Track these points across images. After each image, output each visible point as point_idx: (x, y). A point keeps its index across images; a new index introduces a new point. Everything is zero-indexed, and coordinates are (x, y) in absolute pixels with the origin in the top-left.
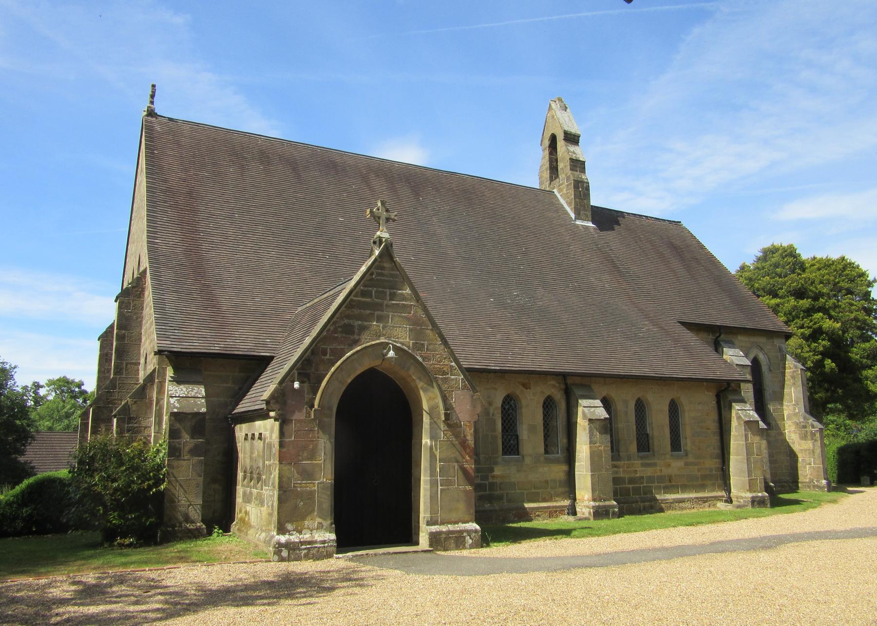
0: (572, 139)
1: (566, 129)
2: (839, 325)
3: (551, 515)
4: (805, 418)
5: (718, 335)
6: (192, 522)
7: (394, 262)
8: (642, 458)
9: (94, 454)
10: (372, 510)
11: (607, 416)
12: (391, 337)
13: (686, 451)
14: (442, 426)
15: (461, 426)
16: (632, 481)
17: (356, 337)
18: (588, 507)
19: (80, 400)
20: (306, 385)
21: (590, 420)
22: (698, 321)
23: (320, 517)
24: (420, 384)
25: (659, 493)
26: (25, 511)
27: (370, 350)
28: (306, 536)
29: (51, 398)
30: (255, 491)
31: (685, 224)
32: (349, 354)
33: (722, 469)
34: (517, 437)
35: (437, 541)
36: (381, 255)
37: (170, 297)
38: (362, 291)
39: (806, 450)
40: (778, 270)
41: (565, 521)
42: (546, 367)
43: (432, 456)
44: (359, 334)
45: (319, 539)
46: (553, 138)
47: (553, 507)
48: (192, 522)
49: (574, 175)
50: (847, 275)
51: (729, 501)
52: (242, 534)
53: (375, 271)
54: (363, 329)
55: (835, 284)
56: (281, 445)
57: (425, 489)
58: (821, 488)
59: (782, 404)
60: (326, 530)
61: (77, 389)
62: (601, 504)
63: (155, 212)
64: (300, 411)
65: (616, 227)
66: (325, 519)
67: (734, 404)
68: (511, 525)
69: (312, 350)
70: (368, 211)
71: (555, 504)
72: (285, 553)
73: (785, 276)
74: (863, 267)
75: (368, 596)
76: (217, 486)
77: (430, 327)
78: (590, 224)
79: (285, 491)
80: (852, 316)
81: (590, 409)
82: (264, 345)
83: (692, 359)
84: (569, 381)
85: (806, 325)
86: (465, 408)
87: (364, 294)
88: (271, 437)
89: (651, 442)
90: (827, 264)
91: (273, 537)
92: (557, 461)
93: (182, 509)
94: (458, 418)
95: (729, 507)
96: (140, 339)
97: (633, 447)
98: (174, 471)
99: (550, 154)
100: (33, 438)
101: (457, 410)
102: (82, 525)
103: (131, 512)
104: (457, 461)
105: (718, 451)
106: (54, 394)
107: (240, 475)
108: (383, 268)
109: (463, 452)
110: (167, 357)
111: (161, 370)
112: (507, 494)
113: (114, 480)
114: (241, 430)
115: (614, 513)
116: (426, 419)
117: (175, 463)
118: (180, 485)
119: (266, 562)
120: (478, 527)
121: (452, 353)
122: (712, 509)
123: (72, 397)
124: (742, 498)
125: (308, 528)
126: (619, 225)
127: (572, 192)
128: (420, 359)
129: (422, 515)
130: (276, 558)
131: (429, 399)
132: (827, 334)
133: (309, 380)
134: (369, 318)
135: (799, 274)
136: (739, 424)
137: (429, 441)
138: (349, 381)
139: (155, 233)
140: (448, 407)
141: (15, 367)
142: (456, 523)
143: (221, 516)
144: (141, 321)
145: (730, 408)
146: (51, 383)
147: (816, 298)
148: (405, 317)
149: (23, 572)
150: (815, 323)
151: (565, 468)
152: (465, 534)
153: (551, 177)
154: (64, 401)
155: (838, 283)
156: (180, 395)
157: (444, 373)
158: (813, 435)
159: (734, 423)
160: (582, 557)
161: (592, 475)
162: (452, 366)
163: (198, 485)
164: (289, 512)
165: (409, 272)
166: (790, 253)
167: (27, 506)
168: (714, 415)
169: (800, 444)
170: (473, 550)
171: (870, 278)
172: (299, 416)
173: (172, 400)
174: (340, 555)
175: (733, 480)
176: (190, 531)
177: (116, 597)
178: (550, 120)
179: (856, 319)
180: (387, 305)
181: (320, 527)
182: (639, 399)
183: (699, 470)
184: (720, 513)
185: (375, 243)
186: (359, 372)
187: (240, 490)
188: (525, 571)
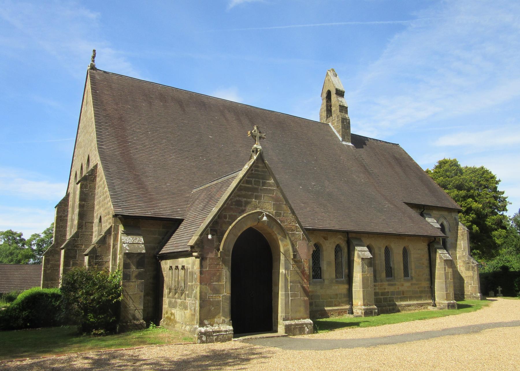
0: (340, 93)
2: (481, 206)
3: (339, 314)
4: (469, 258)
5: (423, 210)
6: (138, 320)
7: (265, 163)
8: (388, 281)
9: (77, 279)
10: (252, 313)
11: (372, 256)
12: (265, 208)
14: (291, 261)
15: (302, 262)
16: (383, 294)
17: (243, 208)
18: (361, 309)
19: (20, 245)
20: (215, 236)
21: (363, 259)
22: (412, 202)
24: (279, 237)
26: (25, 313)
28: (216, 328)
30: (179, 301)
31: (401, 145)
33: (431, 287)
34: (320, 268)
35: (289, 330)
36: (257, 159)
37: (117, 182)
38: (247, 180)
39: (469, 277)
40: (448, 174)
41: (347, 318)
42: (337, 227)
44: (245, 207)
45: (224, 329)
46: (329, 93)
47: (341, 309)
48: (138, 320)
49: (341, 115)
50: (485, 177)
51: (435, 305)
52: (170, 327)
54: (247, 203)
55: (478, 182)
56: (201, 273)
59: (456, 250)
60: (227, 324)
62: (368, 307)
63: (101, 129)
64: (212, 252)
65: (364, 146)
66: (226, 318)
68: (318, 320)
69: (219, 216)
70: (249, 132)
71: (341, 308)
72: (204, 338)
73: (452, 177)
74: (493, 173)
75: (272, 363)
76: (149, 298)
77: (285, 203)
78: (350, 144)
80: (487, 201)
81: (361, 253)
82: (177, 212)
83: (410, 224)
84: (350, 235)
85: (463, 205)
86: (305, 252)
87: (248, 182)
88: (193, 268)
89: (393, 271)
90: (474, 171)
91: (196, 328)
92: (342, 283)
93: (131, 312)
94: (300, 257)
95: (435, 309)
96: (94, 207)
97: (384, 275)
98: (127, 289)
99: (327, 102)
101: (300, 252)
102: (67, 321)
103: (100, 314)
104: (300, 283)
105: (429, 277)
107: (166, 291)
108: (258, 167)
109: (303, 278)
110: (119, 218)
111: (116, 227)
112: (315, 302)
113: (91, 294)
114: (166, 264)
115: (375, 313)
116: (282, 258)
117: (127, 284)
118: (130, 297)
119: (193, 343)
120: (311, 322)
121: (297, 219)
122: (426, 310)
124: (442, 304)
125: (217, 323)
126: (366, 145)
128: (279, 222)
130: (199, 341)
131: (285, 246)
132: (474, 210)
133: (217, 233)
134: (250, 197)
135: (459, 176)
136: (441, 261)
137: (284, 271)
138: (239, 234)
139: (102, 142)
140: (295, 251)
142: (299, 319)
143: (154, 315)
144: (94, 196)
145: (436, 252)
147: (468, 190)
148: (271, 197)
149: (48, 351)
150: (468, 204)
151: (347, 286)
152: (304, 326)
153: (327, 116)
154: (10, 245)
155: (480, 181)
156: (128, 242)
157: (292, 230)
158: (473, 268)
159: (438, 261)
160: (375, 338)
161: (363, 291)
162: (296, 226)
163: (140, 297)
164: (206, 313)
166: (454, 164)
167: (25, 311)
168: (426, 256)
169: (465, 273)
170: (309, 335)
171: (497, 179)
172: (211, 255)
173: (124, 245)
174: (236, 339)
175: (437, 294)
176: (136, 325)
177: (118, 366)
178: (327, 82)
179: (489, 202)
181: (224, 322)
183: (418, 288)
184: (432, 312)
185: (253, 151)
186: (245, 229)
187: (166, 301)
188: (352, 347)
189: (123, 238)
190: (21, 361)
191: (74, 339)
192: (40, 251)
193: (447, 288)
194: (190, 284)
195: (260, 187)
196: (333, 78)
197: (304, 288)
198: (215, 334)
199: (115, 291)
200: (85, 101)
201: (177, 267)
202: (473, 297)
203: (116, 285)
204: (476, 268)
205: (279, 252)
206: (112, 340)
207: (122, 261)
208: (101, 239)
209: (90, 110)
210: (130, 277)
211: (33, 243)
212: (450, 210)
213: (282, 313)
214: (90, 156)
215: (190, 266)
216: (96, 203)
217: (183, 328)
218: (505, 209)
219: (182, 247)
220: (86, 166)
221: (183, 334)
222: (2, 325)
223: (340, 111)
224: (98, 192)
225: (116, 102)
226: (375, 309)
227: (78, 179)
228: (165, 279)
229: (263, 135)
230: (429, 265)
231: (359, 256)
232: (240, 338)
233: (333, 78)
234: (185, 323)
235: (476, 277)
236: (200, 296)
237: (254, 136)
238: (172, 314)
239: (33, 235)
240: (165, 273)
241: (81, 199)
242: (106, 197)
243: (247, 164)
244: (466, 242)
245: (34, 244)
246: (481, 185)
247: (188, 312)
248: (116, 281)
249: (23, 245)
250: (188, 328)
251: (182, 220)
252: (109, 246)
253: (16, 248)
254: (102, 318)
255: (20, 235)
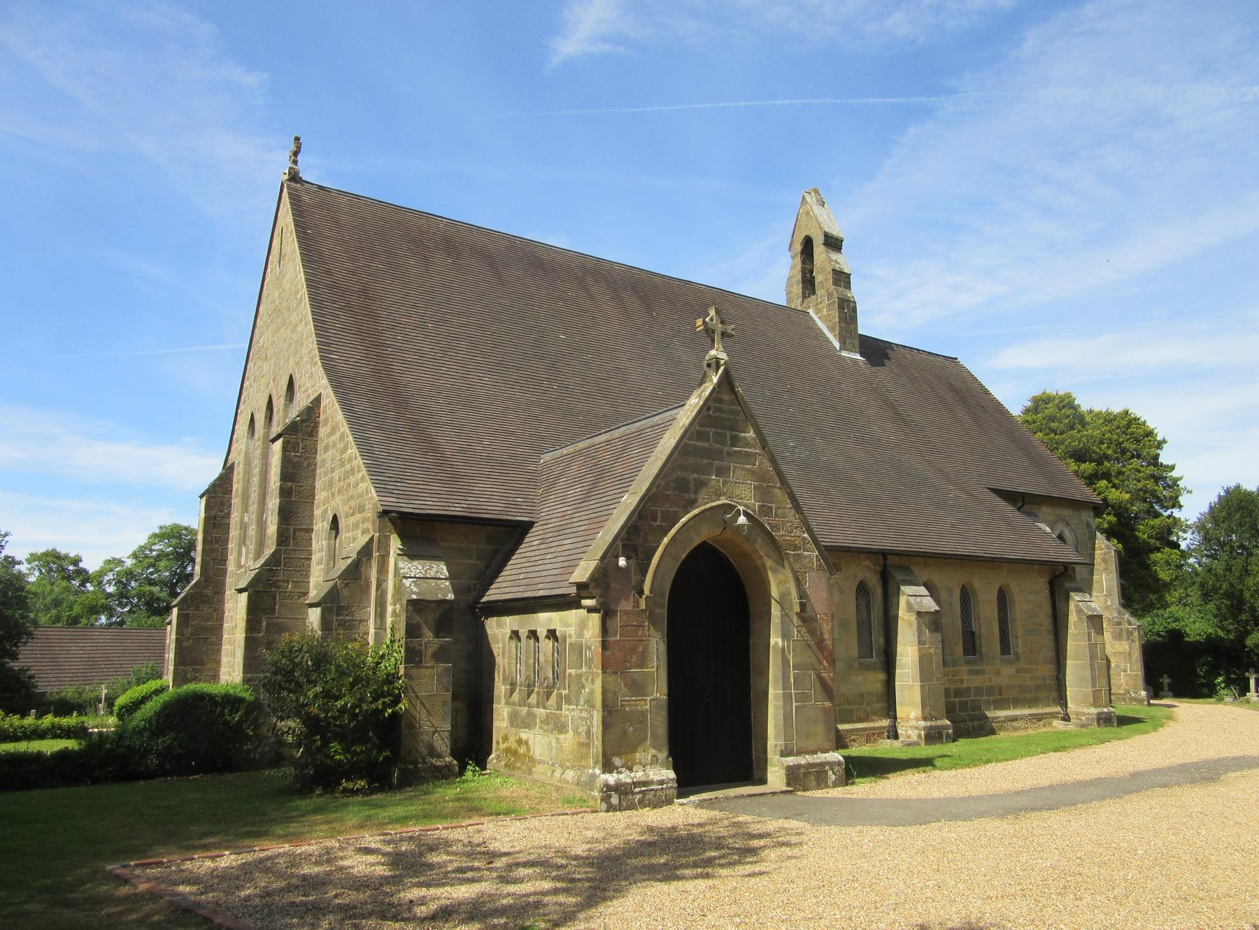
0: (833, 243)
1: (827, 230)
4: (1119, 613)
6: (439, 756)
7: (735, 394)
8: (969, 663)
12: (738, 495)
13: (1017, 654)
14: (795, 619)
16: (958, 693)
17: (692, 496)
18: (917, 728)
19: (76, 583)
20: (633, 561)
21: (919, 613)
23: (655, 748)
24: (769, 563)
25: (989, 709)
26: (163, 742)
27: (708, 514)
28: (639, 775)
29: (32, 579)
30: (540, 712)
31: (963, 361)
32: (684, 520)
35: (796, 778)
38: (698, 432)
39: (1120, 653)
41: (885, 748)
42: (861, 542)
43: (785, 661)
44: (696, 493)
45: (656, 778)
46: (808, 244)
48: (439, 756)
51: (1066, 718)
52: (517, 773)
53: (712, 404)
54: (701, 484)
56: (605, 645)
57: (776, 707)
58: (1139, 701)
60: (662, 765)
61: (71, 568)
62: (934, 723)
64: (627, 599)
65: (886, 361)
66: (660, 751)
67: (1072, 594)
70: (699, 322)
72: (615, 800)
73: (1062, 433)
74: (1151, 424)
79: (610, 712)
81: (913, 600)
87: (700, 436)
88: (581, 634)
89: (977, 642)
90: (1108, 419)
91: (594, 777)
92: (871, 668)
95: (1070, 727)
96: (313, 495)
97: (959, 650)
99: (803, 262)
100: (30, 634)
104: (814, 669)
106: (37, 573)
107: (500, 689)
108: (721, 401)
109: (820, 656)
113: (337, 698)
116: (775, 611)
117: (415, 672)
118: (422, 703)
119: (593, 812)
123: (64, 578)
124: (1084, 714)
125: (640, 763)
127: (835, 314)
129: (771, 742)
131: (780, 583)
132: (1113, 507)
134: (706, 470)
136: (1080, 619)
137: (780, 641)
138: (684, 556)
140: (802, 595)
141: (6, 535)
142: (815, 752)
143: (474, 744)
144: (314, 470)
145: (1067, 598)
146: (33, 558)
147: (1099, 463)
148: (748, 470)
151: (882, 676)
152: (827, 768)
153: (804, 293)
154: (52, 584)
157: (796, 548)
158: (1130, 633)
159: (1073, 618)
161: (922, 686)
164: (616, 744)
165: (756, 410)
166: (1067, 403)
167: (164, 735)
168: (1047, 608)
171: (1159, 438)
173: (407, 582)
174: (684, 801)
176: (437, 768)
180: (730, 454)
181: (655, 761)
182: (861, 582)
183: (1032, 679)
184: (1067, 735)
186: (695, 544)
189: (401, 564)
190: (213, 858)
191: (299, 802)
192: (123, 595)
193: (1093, 679)
194: (573, 671)
195: (726, 449)
196: (817, 209)
197: (823, 682)
198: (637, 790)
199: (387, 687)
200: (275, 251)
201: (533, 634)
202: (1132, 699)
203: (388, 675)
204: (1136, 634)
205: (769, 596)
206: (397, 805)
207: (403, 617)
208: (349, 566)
209: (292, 274)
210: (421, 657)
211: (106, 578)
212: (1076, 505)
213: (776, 738)
214: (296, 378)
215: (571, 631)
216: (318, 484)
217: (557, 774)
218: (1176, 504)
219: (548, 586)
220: (282, 400)
221: (558, 789)
222: (111, 768)
223: (834, 284)
224: (324, 461)
225: (361, 258)
226: (946, 727)
227: (276, 429)
228: (499, 661)
229: (729, 328)
230: (1051, 627)
231: (910, 607)
232: (692, 798)
233: (817, 209)
234: (557, 768)
235: (1137, 654)
236: (603, 700)
237: (709, 331)
238: (520, 742)
239: (108, 562)
240: (497, 648)
241: (285, 477)
242: (352, 471)
243: (696, 393)
244: (1114, 575)
245: (109, 582)
246: (1124, 452)
247: (568, 739)
248: (387, 666)
249: (83, 584)
250: (570, 775)
251: (530, 525)
252: (368, 584)
253: (67, 589)
254: (362, 752)
255: (76, 561)
